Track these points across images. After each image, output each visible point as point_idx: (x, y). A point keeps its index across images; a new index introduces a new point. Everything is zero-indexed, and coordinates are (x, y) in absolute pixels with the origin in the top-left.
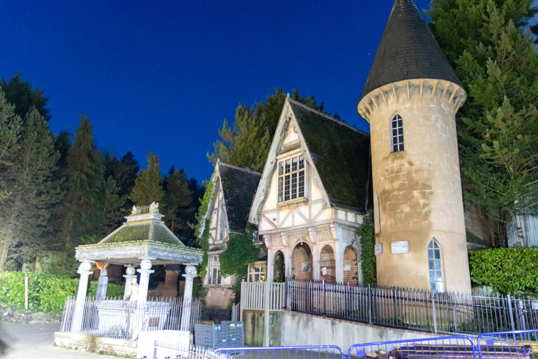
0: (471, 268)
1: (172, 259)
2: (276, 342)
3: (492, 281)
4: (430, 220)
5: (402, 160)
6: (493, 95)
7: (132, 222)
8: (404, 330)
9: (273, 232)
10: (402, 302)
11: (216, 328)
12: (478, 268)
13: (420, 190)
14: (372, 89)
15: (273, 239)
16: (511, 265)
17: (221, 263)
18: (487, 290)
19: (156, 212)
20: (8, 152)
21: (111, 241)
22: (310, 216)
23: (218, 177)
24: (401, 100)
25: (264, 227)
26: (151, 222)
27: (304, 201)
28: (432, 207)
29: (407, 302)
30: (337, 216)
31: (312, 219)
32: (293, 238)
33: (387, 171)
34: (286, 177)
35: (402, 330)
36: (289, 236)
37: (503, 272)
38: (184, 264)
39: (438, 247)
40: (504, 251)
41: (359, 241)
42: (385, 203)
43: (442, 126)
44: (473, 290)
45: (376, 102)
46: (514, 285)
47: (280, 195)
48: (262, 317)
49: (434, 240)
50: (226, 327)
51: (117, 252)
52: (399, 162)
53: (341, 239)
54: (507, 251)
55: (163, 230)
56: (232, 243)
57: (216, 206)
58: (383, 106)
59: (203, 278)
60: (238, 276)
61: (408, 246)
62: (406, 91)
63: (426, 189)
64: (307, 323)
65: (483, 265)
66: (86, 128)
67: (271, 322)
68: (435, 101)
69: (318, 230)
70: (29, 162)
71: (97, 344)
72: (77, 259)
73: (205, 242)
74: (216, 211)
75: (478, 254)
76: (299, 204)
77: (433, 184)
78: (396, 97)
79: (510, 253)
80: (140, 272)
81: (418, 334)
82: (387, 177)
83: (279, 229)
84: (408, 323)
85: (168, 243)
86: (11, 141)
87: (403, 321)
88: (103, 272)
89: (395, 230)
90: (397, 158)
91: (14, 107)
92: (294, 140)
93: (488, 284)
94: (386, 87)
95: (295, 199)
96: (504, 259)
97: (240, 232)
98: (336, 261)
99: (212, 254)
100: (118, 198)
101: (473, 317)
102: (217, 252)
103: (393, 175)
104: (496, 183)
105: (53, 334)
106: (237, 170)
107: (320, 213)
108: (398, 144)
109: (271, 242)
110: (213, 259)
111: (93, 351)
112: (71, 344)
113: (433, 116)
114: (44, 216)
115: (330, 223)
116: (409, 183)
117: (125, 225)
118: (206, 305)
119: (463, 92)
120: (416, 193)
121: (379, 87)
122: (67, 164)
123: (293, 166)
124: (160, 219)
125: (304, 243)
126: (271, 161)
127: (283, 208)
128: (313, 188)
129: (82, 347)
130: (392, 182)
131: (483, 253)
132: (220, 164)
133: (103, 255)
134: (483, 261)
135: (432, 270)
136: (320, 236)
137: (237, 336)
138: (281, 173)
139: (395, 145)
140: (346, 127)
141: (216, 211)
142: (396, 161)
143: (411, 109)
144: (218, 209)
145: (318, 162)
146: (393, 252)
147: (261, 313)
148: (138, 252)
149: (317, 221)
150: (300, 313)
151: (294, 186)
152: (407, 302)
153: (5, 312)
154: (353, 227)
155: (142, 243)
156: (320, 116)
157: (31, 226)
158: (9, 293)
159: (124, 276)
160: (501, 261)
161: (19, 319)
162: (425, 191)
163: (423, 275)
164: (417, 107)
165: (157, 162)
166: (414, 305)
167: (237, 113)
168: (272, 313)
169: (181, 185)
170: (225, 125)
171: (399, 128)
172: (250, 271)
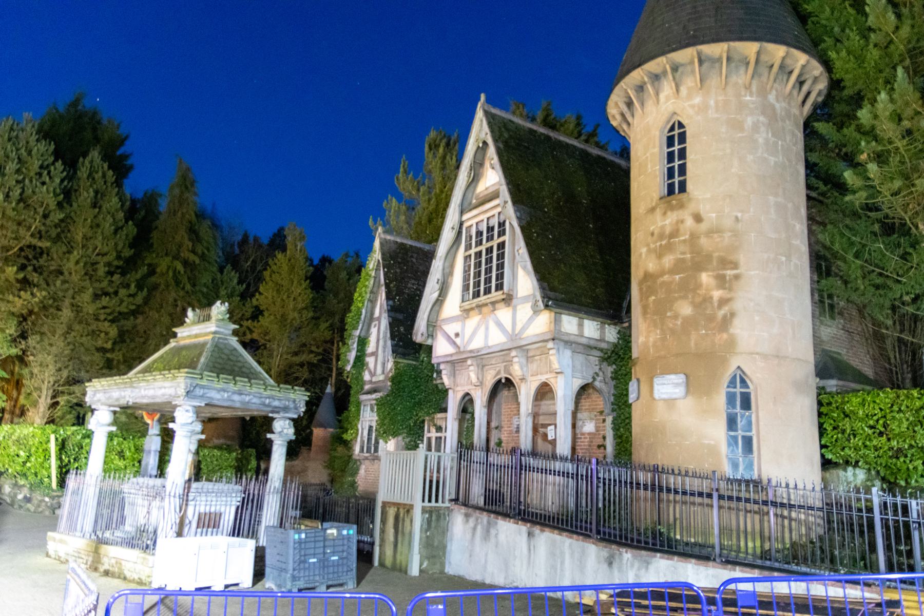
0: (822, 432)
1: (238, 405)
2: (434, 564)
3: (864, 456)
4: (732, 331)
5: (680, 212)
6: (881, 71)
7: (184, 338)
8: (653, 554)
9: (454, 358)
10: (668, 497)
11: (296, 536)
12: (836, 431)
13: (713, 271)
14: (628, 72)
15: (457, 372)
16: (905, 424)
17: (378, 415)
18: (854, 475)
19: (223, 320)
20: (44, 224)
21: (145, 371)
22: (524, 328)
23: (379, 261)
24: (684, 90)
25: (442, 349)
26: (211, 337)
27: (503, 299)
28: (737, 305)
29: (671, 497)
30: (560, 327)
31: (517, 332)
32: (490, 369)
33: (652, 234)
34: (476, 253)
35: (649, 553)
36: (482, 367)
37: (889, 440)
38: (270, 415)
39: (748, 387)
40: (891, 396)
41: (609, 375)
42: (647, 298)
43: (767, 140)
44: (828, 475)
45: (638, 98)
46: (911, 467)
47: (466, 288)
48: (409, 516)
49: (739, 372)
50: (317, 534)
51: (143, 392)
52: (675, 215)
53: (569, 371)
54: (898, 397)
55: (234, 352)
56: (397, 379)
57: (377, 313)
58: (650, 105)
59: (353, 442)
60: (408, 440)
61: (684, 385)
62: (693, 72)
63: (728, 269)
64: (488, 531)
65: (847, 425)
66: (186, 183)
67: (425, 526)
68: (754, 88)
69: (531, 354)
70: (82, 242)
71: (101, 556)
72: (88, 405)
73: (357, 378)
74: (377, 322)
75: (836, 402)
76: (497, 306)
77: (742, 258)
78: (673, 85)
79: (903, 401)
80: (175, 429)
81: (681, 563)
82: (652, 246)
83: (464, 352)
84: (678, 537)
85: (230, 375)
86: (48, 205)
87: (669, 533)
88: (152, 428)
89: (663, 353)
90: (672, 208)
91: (53, 147)
92: (492, 182)
93: (856, 465)
94: (653, 66)
95: (489, 296)
96: (892, 411)
97: (412, 360)
98: (558, 415)
99: (366, 400)
100: (241, 303)
101: (821, 531)
102: (374, 396)
103: (664, 243)
104: (884, 255)
105: (46, 534)
106: (416, 247)
107: (531, 320)
108: (677, 180)
109: (454, 376)
110: (369, 408)
111: (96, 569)
112: (68, 554)
113: (749, 121)
114: (107, 334)
115: (546, 341)
116: (692, 258)
117: (173, 343)
118: (356, 490)
119: (817, 69)
120: (705, 278)
121: (639, 65)
122: (152, 244)
123: (488, 232)
124: (231, 332)
125: (507, 379)
126: (451, 226)
127: (471, 313)
128: (521, 273)
129: (81, 560)
130: (660, 256)
131: (846, 399)
132: (383, 236)
133: (124, 397)
134: (847, 416)
135: (732, 433)
136: (534, 366)
137: (343, 551)
138: (468, 247)
139: (670, 181)
140: (604, 159)
141: (377, 322)
142: (669, 213)
143: (703, 109)
144: (379, 319)
145: (529, 224)
146: (656, 396)
147: (409, 509)
148: (171, 391)
149: (524, 336)
150: (478, 511)
151: (489, 271)
152: (678, 497)
153: (20, 493)
154: (596, 348)
155: (176, 375)
156: (548, 138)
157: (87, 350)
158: (30, 462)
159: (269, 436)
160: (885, 417)
161: (39, 506)
162: (725, 272)
163: (712, 442)
164: (716, 102)
165: (302, 238)
166: (700, 504)
167: (427, 146)
168: (428, 509)
169: (349, 279)
170: (404, 166)
171: (680, 147)
172: (429, 431)
